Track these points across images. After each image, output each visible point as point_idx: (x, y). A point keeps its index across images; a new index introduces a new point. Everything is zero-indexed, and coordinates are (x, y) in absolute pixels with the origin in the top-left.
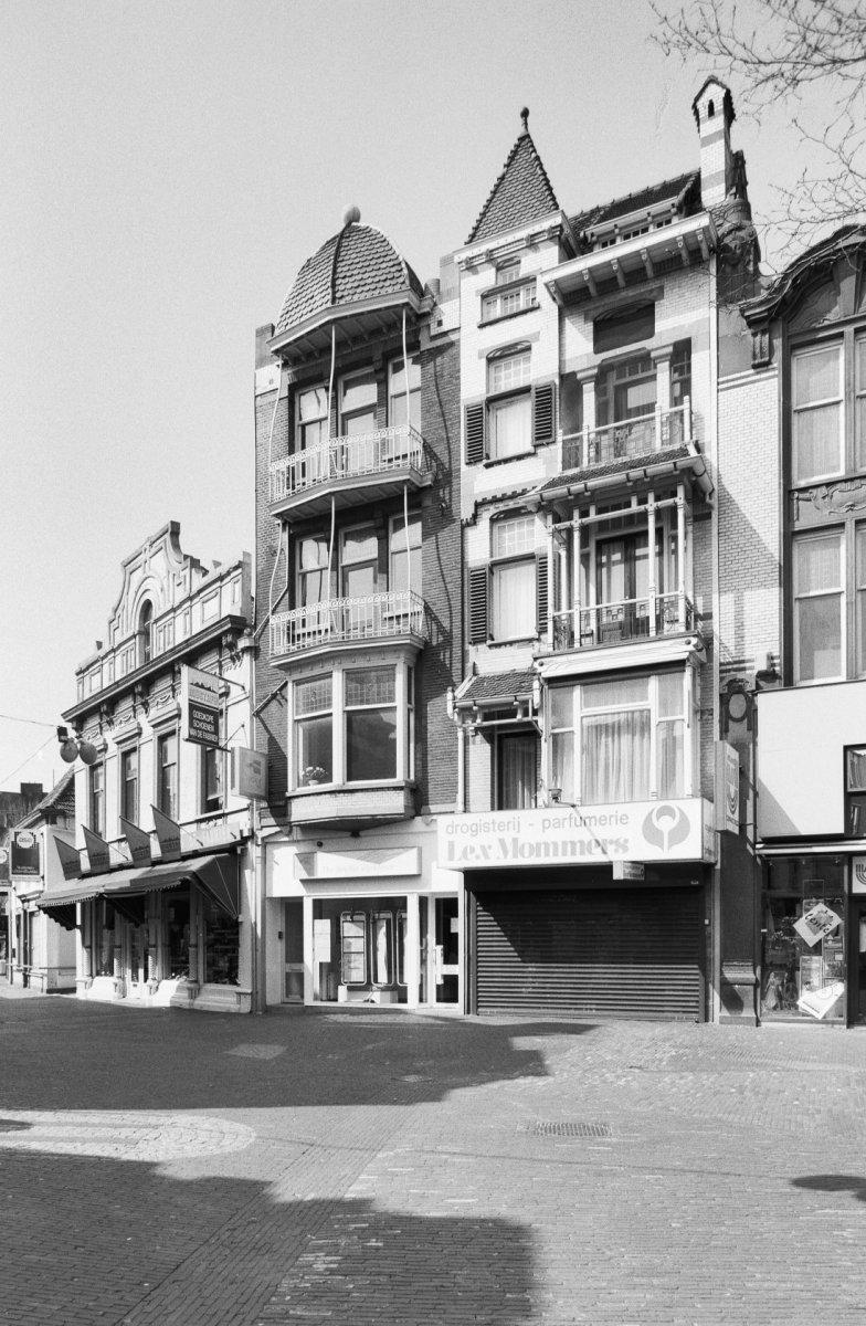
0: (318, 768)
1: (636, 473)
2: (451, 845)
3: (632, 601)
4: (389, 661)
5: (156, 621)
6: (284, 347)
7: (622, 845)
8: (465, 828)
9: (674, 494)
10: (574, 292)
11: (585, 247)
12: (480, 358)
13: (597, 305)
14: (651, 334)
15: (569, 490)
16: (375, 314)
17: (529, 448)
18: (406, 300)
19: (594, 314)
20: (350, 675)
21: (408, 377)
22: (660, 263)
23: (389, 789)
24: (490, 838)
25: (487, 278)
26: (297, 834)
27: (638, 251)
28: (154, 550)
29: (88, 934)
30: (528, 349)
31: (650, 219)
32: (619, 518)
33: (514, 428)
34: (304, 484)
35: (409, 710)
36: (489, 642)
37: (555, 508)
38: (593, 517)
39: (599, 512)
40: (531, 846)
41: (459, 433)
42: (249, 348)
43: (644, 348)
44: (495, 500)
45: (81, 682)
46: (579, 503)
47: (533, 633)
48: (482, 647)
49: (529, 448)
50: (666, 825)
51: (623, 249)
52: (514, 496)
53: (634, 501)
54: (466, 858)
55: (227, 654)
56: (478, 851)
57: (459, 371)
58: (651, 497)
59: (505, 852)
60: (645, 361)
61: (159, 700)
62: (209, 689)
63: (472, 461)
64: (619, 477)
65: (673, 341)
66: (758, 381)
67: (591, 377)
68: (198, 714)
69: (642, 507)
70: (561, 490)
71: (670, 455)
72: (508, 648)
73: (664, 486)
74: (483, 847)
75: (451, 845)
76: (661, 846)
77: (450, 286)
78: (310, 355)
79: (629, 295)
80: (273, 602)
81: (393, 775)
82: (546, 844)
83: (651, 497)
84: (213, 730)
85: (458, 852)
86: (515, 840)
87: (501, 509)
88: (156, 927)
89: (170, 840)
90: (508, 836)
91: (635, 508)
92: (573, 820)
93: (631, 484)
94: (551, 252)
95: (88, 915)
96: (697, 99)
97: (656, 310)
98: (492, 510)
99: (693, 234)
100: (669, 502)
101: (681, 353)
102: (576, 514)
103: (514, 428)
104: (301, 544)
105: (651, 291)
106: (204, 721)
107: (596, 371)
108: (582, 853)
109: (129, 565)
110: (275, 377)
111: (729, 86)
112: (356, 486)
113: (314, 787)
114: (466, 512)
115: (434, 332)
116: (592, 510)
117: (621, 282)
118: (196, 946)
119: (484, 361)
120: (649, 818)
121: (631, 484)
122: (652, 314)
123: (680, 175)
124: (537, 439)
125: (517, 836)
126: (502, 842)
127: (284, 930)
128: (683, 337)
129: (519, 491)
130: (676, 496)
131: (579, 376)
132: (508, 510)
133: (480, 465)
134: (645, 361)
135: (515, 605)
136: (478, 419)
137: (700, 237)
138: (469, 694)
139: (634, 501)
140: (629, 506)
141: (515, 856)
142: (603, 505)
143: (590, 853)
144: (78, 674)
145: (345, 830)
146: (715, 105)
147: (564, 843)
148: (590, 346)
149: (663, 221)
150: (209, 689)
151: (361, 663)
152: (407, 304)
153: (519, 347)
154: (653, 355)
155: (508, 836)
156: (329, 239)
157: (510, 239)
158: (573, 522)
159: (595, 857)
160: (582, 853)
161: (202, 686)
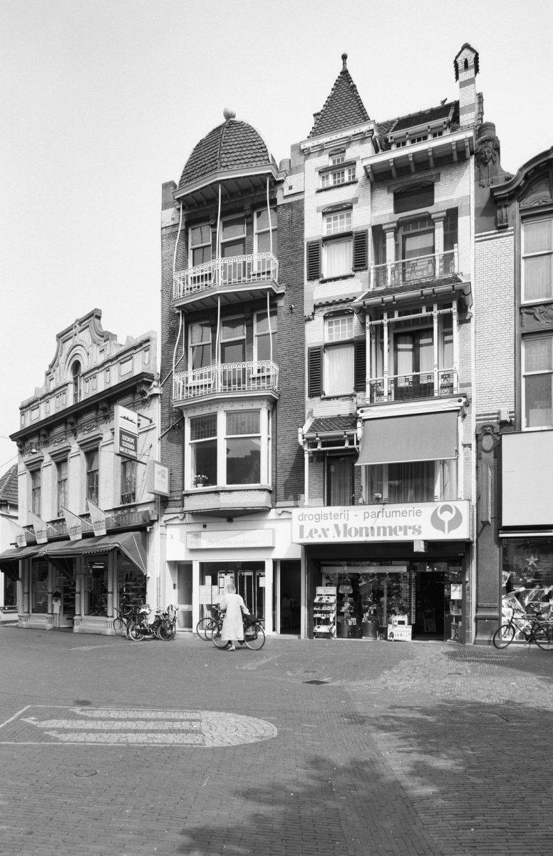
0: (203, 476)
1: (427, 291)
2: (302, 528)
3: (396, 376)
4: (256, 405)
5: (83, 375)
6: (183, 196)
7: (417, 530)
8: (311, 517)
9: (451, 306)
10: (381, 173)
11: (386, 146)
12: (318, 211)
13: (397, 182)
14: (431, 203)
15: (382, 299)
16: (247, 179)
17: (349, 271)
18: (270, 171)
19: (394, 188)
20: (228, 414)
21: (267, 221)
22: (438, 158)
23: (211, 492)
24: (329, 524)
25: (325, 161)
26: (189, 519)
27: (388, 160)
28: (82, 327)
29: (26, 584)
30: (350, 208)
31: (429, 130)
32: (409, 320)
33: (336, 260)
34: (198, 287)
35: (269, 439)
36: (323, 396)
37: (370, 311)
38: (396, 318)
39: (400, 315)
40: (356, 529)
41: (303, 260)
42: (157, 196)
43: (427, 212)
44: (328, 304)
45: (22, 414)
46: (389, 308)
47: (350, 389)
48: (317, 399)
49: (349, 271)
50: (446, 517)
51: (410, 150)
52: (348, 301)
53: (424, 309)
54: (312, 537)
55: (138, 397)
56: (320, 532)
57: (303, 219)
58: (435, 307)
59: (339, 533)
60: (428, 220)
61: (85, 428)
62: (131, 421)
63: (311, 278)
64: (417, 293)
65: (446, 209)
66: (500, 237)
67: (392, 228)
68: (125, 437)
69: (430, 313)
70: (377, 300)
71: (447, 281)
72: (336, 401)
73: (444, 301)
74: (323, 530)
75: (302, 528)
76: (443, 531)
77: (297, 164)
78: (200, 203)
79: (417, 178)
80: (176, 361)
81: (257, 480)
82: (366, 528)
83: (435, 307)
84: (134, 448)
85: (306, 533)
86: (345, 526)
87: (331, 310)
88: (80, 579)
89: (99, 522)
90: (341, 523)
91: (424, 313)
92: (384, 513)
93: (434, 296)
94: (368, 147)
95: (26, 570)
96: (457, 57)
97: (435, 188)
98: (326, 310)
99: (462, 141)
100: (447, 311)
101: (451, 217)
102: (385, 316)
103: (336, 260)
104: (192, 327)
105: (432, 176)
106: (128, 442)
107: (444, 214)
108: (391, 534)
109: (63, 337)
110: (172, 216)
111: (477, 51)
112: (209, 295)
113: (201, 488)
114: (308, 310)
115: (287, 192)
116: (396, 314)
117: (413, 169)
118: (80, 593)
119: (321, 214)
120: (435, 513)
121: (423, 297)
122: (433, 190)
123: (429, 107)
124: (356, 266)
125: (347, 522)
126: (336, 526)
127: (176, 583)
128: (454, 206)
129: (351, 298)
130: (451, 307)
131: (384, 227)
132: (336, 311)
133: (317, 282)
134: (428, 220)
135: (337, 372)
136: (314, 251)
137: (467, 144)
138: (310, 431)
139: (424, 309)
140: (393, 317)
141: (345, 536)
142: (403, 309)
143: (312, 537)
144: (21, 409)
145: (222, 517)
146: (469, 62)
147: (379, 528)
148: (392, 210)
149: (437, 133)
150: (131, 421)
151: (237, 407)
152: (270, 174)
153: (344, 206)
154: (433, 216)
155: (341, 523)
156: (215, 128)
157: (339, 136)
158: (383, 321)
159: (400, 537)
160: (391, 534)
161: (127, 419)
